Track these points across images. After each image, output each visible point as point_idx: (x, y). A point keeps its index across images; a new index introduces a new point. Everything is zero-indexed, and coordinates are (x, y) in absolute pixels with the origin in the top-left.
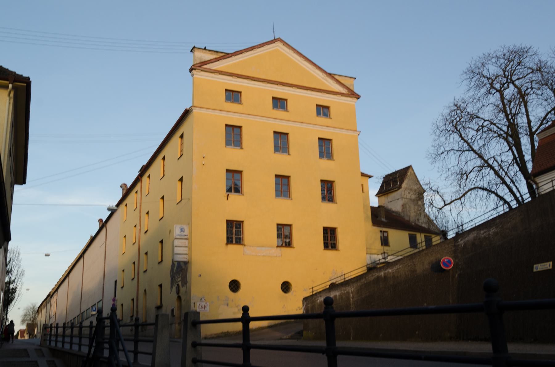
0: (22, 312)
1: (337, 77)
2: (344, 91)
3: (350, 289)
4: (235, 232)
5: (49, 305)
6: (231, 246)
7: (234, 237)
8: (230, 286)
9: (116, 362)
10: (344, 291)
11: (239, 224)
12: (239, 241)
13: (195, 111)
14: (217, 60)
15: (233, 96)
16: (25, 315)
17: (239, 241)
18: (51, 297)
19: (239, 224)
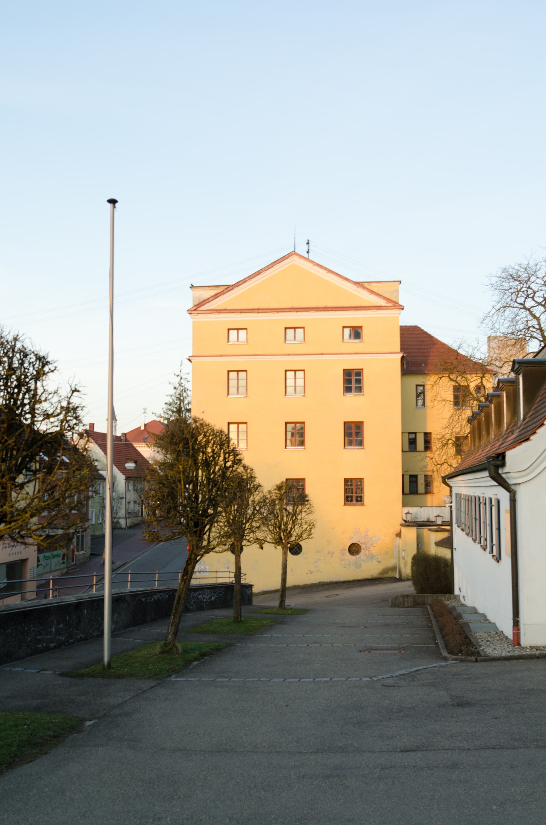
1: (372, 287)
2: (383, 303)
14: (216, 296)
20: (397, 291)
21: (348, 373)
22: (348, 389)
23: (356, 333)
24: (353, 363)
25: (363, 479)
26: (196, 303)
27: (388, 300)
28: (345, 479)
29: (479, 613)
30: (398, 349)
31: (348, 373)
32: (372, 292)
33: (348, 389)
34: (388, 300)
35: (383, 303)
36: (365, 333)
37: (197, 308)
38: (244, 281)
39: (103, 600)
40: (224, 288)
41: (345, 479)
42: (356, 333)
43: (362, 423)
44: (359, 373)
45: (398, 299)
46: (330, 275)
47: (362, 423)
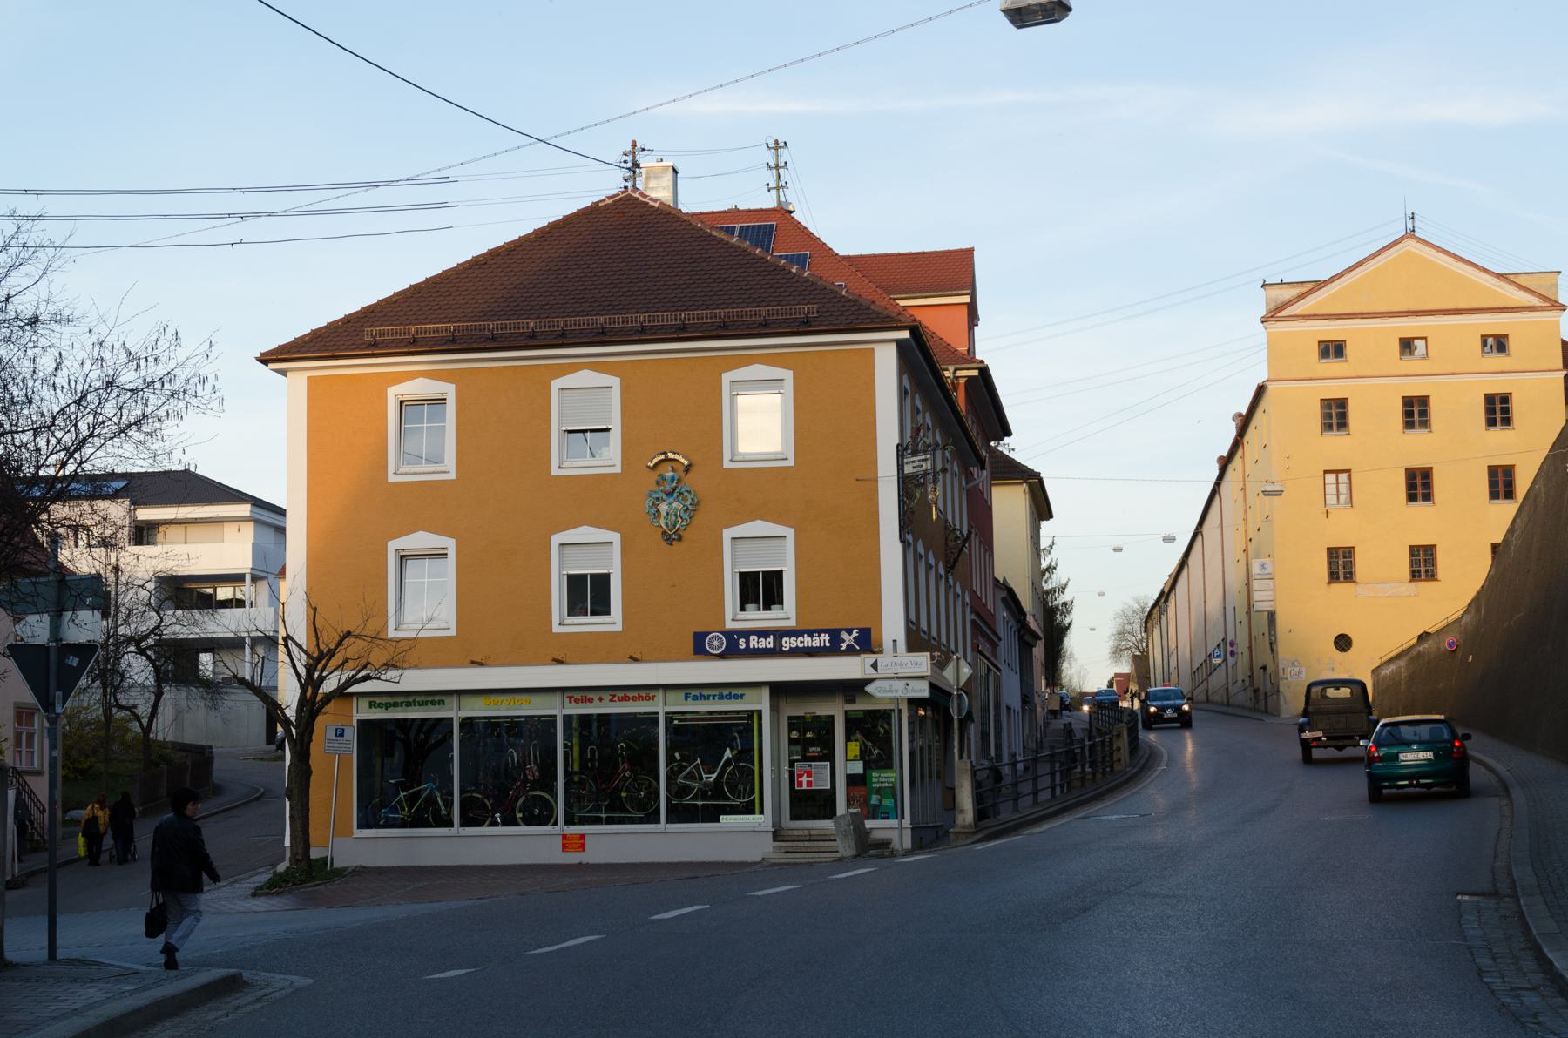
0: (1105, 645)
1: (1521, 280)
2: (1536, 302)
3: (1402, 663)
4: (1341, 565)
5: (1164, 618)
6: (1335, 587)
7: (1341, 571)
8: (1336, 643)
9: (55, 754)
10: (567, 843)
11: (1349, 552)
12: (1349, 577)
13: (1271, 386)
14: (1301, 297)
15: (1333, 350)
16: (1121, 634)
17: (1349, 577)
18: (1167, 600)
19: (1349, 552)
20: (1556, 285)
21: (1408, 402)
22: (1491, 422)
23: (1501, 344)
24: (1498, 385)
25: (1434, 546)
26: (1272, 306)
27: (1544, 298)
28: (1329, 549)
29: (340, 873)
30: (1560, 366)
31: (1408, 402)
32: (1522, 288)
33: (1491, 422)
34: (1544, 298)
35: (1536, 302)
36: (1512, 344)
37: (1274, 314)
38: (1341, 275)
39: (585, 720)
40: (1309, 286)
41: (1329, 549)
42: (1501, 344)
43: (1513, 467)
44: (1424, 401)
45: (1556, 293)
46: (1461, 265)
47: (1513, 467)
